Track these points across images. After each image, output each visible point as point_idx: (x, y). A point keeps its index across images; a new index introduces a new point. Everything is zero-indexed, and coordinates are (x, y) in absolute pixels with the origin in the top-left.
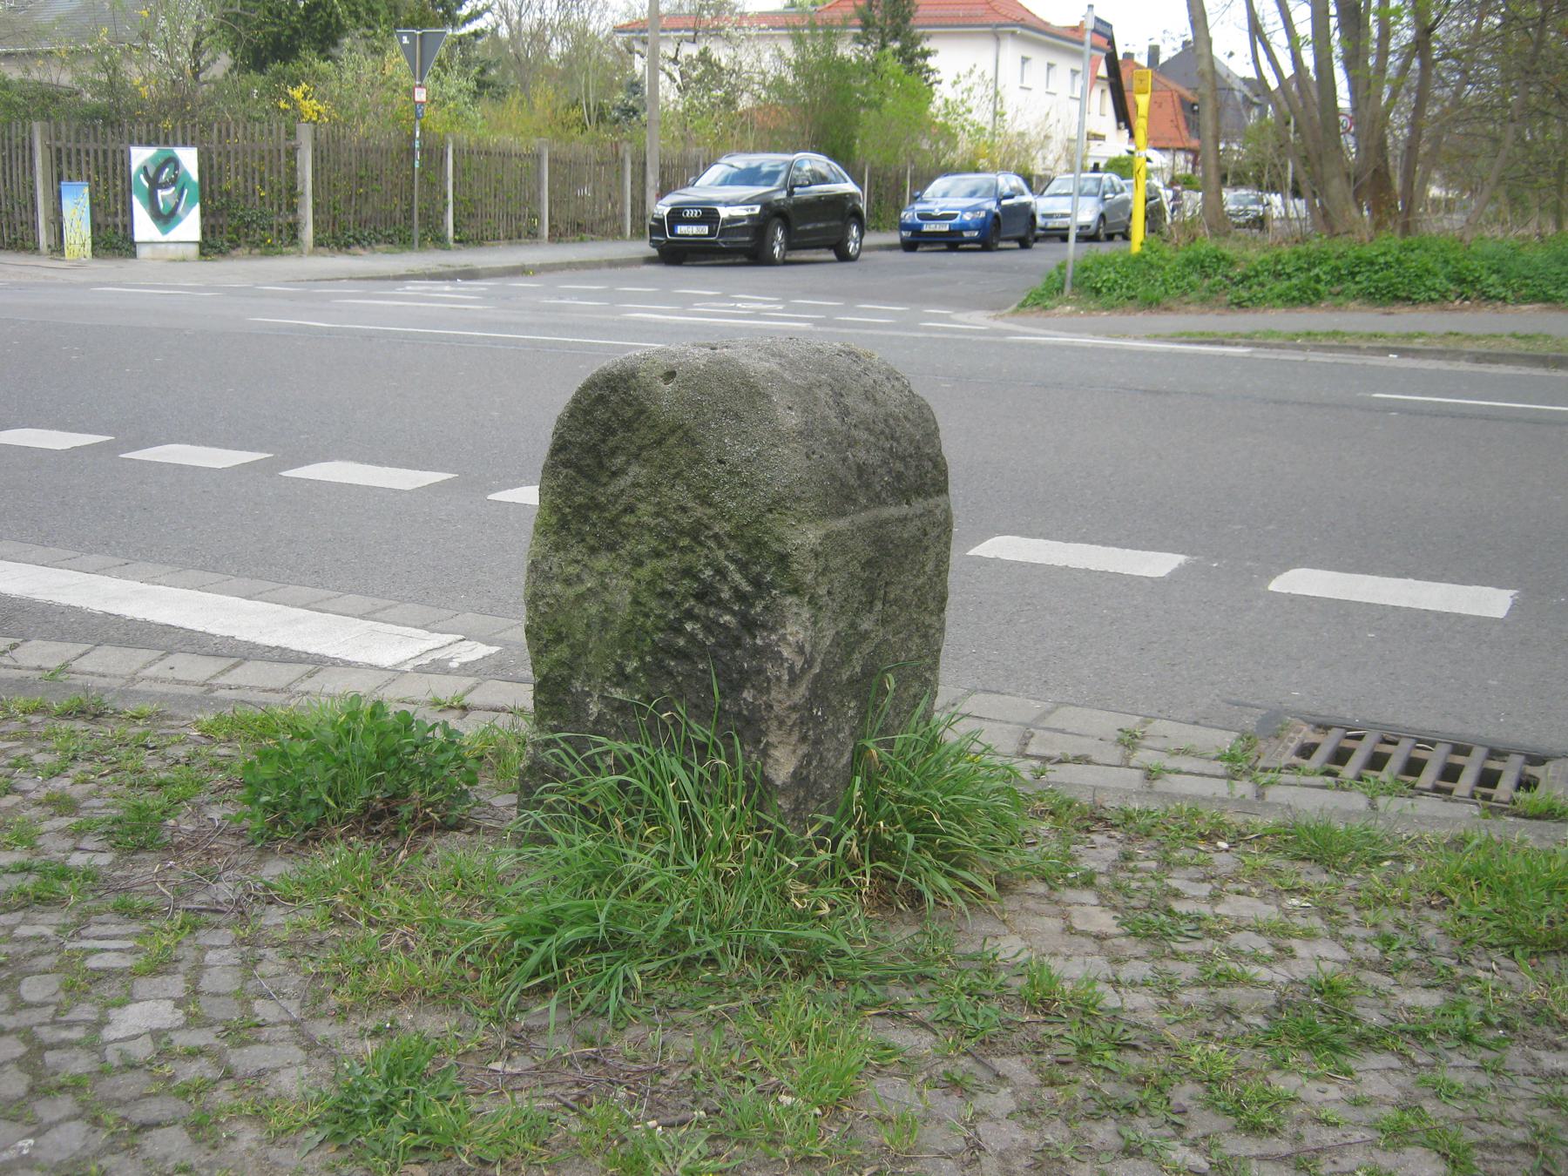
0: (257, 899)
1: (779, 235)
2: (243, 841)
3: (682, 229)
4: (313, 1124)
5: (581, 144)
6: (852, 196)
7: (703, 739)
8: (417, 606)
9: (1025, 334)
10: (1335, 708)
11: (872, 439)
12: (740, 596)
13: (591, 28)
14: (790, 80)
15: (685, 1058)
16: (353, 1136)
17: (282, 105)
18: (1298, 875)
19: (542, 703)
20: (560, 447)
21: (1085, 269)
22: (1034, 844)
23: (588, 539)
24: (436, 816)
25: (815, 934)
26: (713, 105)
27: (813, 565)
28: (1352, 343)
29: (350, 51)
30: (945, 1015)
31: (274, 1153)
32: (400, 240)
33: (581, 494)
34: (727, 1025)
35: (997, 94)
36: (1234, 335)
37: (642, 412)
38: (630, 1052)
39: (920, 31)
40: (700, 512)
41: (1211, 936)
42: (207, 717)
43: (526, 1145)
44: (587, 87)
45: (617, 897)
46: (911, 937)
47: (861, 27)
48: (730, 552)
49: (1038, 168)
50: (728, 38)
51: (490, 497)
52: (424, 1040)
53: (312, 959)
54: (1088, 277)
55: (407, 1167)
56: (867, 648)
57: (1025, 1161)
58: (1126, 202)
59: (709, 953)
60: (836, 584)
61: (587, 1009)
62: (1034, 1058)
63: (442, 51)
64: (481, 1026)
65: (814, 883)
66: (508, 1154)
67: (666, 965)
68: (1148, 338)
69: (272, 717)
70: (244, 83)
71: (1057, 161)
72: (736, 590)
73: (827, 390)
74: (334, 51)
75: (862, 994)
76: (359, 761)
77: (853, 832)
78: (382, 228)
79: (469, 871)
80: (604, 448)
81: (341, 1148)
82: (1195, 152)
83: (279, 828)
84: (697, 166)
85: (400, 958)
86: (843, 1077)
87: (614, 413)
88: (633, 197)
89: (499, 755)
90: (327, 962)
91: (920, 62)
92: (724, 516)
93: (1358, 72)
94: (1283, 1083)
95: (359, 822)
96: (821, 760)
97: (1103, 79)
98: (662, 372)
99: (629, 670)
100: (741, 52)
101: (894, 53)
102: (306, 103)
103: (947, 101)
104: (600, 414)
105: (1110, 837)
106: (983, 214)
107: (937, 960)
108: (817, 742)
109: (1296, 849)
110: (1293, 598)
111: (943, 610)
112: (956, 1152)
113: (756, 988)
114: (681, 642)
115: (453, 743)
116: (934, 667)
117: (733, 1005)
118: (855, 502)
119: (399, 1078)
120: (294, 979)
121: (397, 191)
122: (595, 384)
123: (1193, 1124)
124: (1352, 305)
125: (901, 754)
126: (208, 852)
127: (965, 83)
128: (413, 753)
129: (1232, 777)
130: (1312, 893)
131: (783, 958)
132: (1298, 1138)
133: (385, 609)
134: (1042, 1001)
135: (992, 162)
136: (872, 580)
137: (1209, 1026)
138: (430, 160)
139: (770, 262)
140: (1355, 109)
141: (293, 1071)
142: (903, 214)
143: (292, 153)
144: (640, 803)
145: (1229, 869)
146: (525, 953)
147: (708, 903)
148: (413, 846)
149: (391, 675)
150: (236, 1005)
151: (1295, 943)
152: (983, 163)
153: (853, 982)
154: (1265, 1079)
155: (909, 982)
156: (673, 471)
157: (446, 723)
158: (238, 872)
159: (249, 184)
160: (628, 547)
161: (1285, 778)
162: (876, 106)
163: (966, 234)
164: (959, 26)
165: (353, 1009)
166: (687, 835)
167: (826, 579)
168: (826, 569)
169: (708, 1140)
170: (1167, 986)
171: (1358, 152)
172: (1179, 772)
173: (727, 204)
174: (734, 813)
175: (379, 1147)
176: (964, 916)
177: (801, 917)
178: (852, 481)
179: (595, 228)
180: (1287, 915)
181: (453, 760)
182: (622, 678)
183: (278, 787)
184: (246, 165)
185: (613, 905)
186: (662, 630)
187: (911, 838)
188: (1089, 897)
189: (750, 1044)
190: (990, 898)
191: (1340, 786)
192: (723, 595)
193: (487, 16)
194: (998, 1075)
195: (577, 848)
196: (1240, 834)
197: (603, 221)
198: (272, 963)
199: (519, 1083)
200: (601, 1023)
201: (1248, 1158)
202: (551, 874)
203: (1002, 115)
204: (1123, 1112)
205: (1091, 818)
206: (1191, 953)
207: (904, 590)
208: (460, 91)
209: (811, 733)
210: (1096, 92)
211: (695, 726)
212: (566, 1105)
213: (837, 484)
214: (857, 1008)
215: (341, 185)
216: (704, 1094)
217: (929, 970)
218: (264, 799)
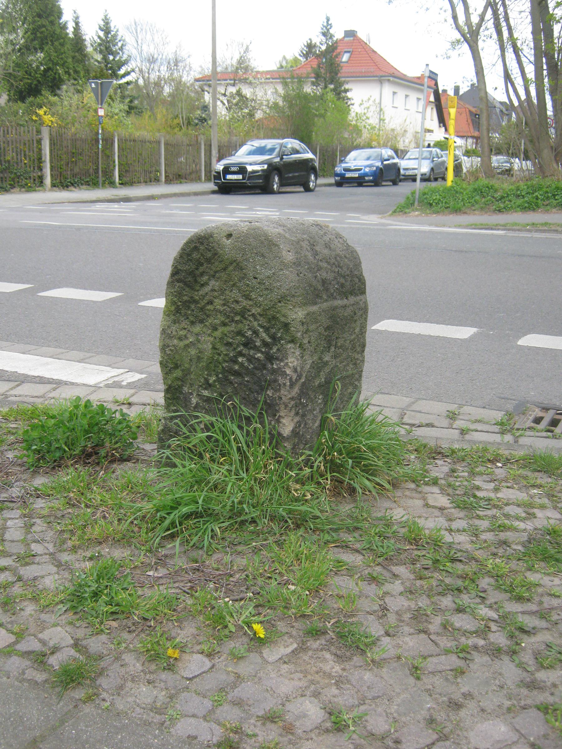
0: (31, 495)
1: (276, 179)
2: (24, 468)
3: (229, 177)
4: (62, 602)
5: (180, 136)
6: (312, 160)
7: (248, 415)
8: (106, 356)
9: (396, 225)
10: (551, 400)
11: (329, 267)
12: (265, 344)
13: (183, 80)
14: (281, 103)
15: (242, 568)
16: (82, 607)
17: (34, 118)
18: (536, 478)
19: (169, 398)
20: (175, 273)
21: (424, 194)
22: (408, 465)
23: (190, 317)
24: (117, 455)
25: (304, 508)
26: (243, 117)
27: (301, 328)
28: (554, 228)
29: (66, 92)
30: (368, 546)
31: (43, 616)
32: (93, 184)
33: (186, 295)
34: (262, 552)
35: (381, 110)
36: (497, 225)
37: (216, 254)
38: (215, 566)
39: (343, 79)
40: (245, 303)
41: (496, 508)
42: (5, 410)
43: (166, 611)
44: (182, 109)
45: (207, 491)
46: (351, 509)
47: (315, 78)
48: (260, 322)
49: (401, 146)
50: (250, 83)
51: (140, 304)
52: (115, 561)
53: (59, 523)
54: (426, 198)
55: (108, 622)
56: (327, 370)
57: (409, 615)
58: (443, 163)
59: (252, 518)
60: (312, 338)
61: (193, 546)
62: (412, 566)
63: (111, 91)
64: (142, 554)
65: (303, 484)
66: (157, 615)
67: (232, 524)
68: (456, 227)
69: (36, 409)
70: (15, 107)
71: (410, 143)
72: (263, 341)
73: (307, 242)
74: (58, 92)
75: (327, 537)
76: (80, 428)
77: (321, 458)
78: (83, 178)
79: (135, 481)
80: (197, 272)
81: (76, 613)
82: (477, 138)
83: (41, 461)
84: (236, 146)
85: (102, 522)
86: (319, 576)
87: (202, 255)
88: (205, 162)
89: (148, 425)
90: (66, 525)
91: (343, 94)
92: (256, 305)
93: (557, 97)
94: (533, 577)
95: (80, 458)
96: (306, 424)
97: (432, 102)
98: (225, 234)
99: (211, 382)
100: (257, 90)
101: (331, 90)
102: (46, 117)
103: (357, 113)
104: (195, 255)
105: (445, 461)
106: (375, 168)
107: (363, 520)
108: (304, 415)
109: (535, 466)
110: (529, 348)
111: (363, 351)
112: (375, 611)
113: (275, 534)
114: (237, 367)
115: (125, 419)
116: (359, 379)
117: (264, 542)
118: (321, 297)
119: (103, 579)
120: (51, 533)
121: (91, 160)
122: (193, 241)
123: (490, 597)
124: (554, 210)
125: (344, 421)
126: (7, 474)
127: (366, 105)
128: (105, 425)
129: (502, 433)
130: (543, 487)
131: (288, 520)
132: (541, 603)
133: (90, 357)
134: (415, 539)
135: (379, 143)
136: (330, 336)
137: (495, 550)
138: (107, 144)
139: (272, 192)
140: (555, 115)
141: (51, 577)
142: (336, 169)
143: (39, 142)
144: (217, 446)
145: (503, 476)
146: (163, 519)
147: (252, 494)
148: (107, 468)
149: (93, 389)
150: (22, 546)
151: (536, 511)
152: (374, 144)
153: (323, 531)
154: (524, 575)
155: (350, 531)
156: (232, 283)
157: (121, 410)
158: (22, 483)
159: (19, 157)
160: (210, 321)
161: (528, 433)
162: (323, 116)
163: (366, 178)
164: (362, 77)
165: (79, 547)
166: (241, 462)
167: (307, 336)
168: (307, 331)
169: (254, 607)
170: (475, 532)
171: (556, 136)
172: (477, 431)
173: (251, 164)
174: (264, 450)
175: (94, 613)
176: (375, 499)
177: (297, 500)
178: (320, 287)
179: (187, 177)
180: (531, 498)
181: (126, 428)
182: (208, 386)
183: (41, 442)
184: (17, 148)
185: (206, 495)
186: (227, 362)
187: (350, 461)
188: (436, 490)
189: (274, 561)
190: (388, 490)
191: (554, 437)
192: (257, 344)
193: (133, 74)
194: (394, 575)
195: (187, 468)
196: (507, 459)
197: (191, 173)
198: (39, 526)
199: (162, 581)
200: (200, 552)
201: (517, 613)
202: (174, 481)
203: (384, 120)
204: (456, 591)
205: (435, 453)
206: (486, 516)
207: (345, 341)
208: (120, 111)
209: (300, 411)
210: (429, 109)
211: (244, 408)
212: (185, 591)
213: (312, 289)
214: (325, 543)
215: (64, 157)
216: (252, 585)
217: (359, 525)
218: (34, 447)
